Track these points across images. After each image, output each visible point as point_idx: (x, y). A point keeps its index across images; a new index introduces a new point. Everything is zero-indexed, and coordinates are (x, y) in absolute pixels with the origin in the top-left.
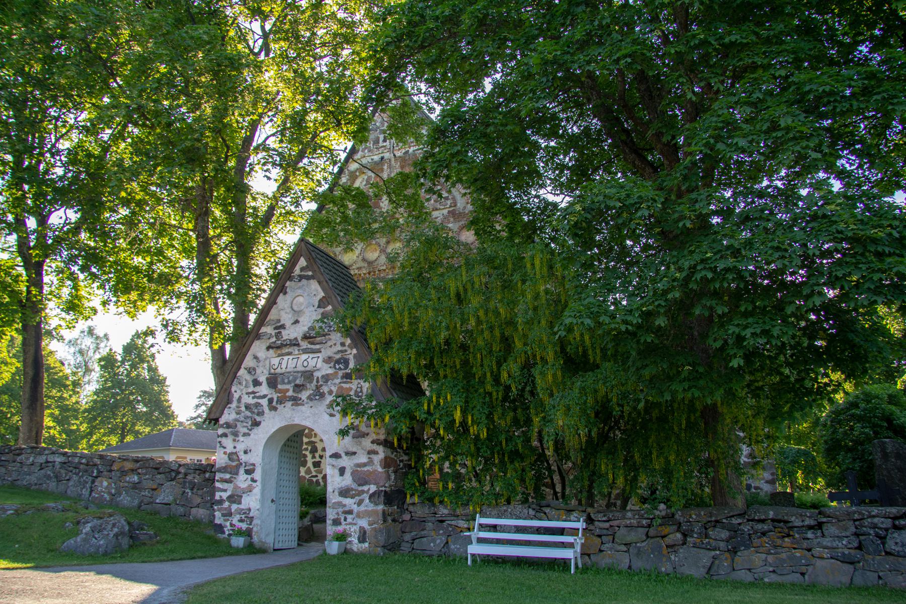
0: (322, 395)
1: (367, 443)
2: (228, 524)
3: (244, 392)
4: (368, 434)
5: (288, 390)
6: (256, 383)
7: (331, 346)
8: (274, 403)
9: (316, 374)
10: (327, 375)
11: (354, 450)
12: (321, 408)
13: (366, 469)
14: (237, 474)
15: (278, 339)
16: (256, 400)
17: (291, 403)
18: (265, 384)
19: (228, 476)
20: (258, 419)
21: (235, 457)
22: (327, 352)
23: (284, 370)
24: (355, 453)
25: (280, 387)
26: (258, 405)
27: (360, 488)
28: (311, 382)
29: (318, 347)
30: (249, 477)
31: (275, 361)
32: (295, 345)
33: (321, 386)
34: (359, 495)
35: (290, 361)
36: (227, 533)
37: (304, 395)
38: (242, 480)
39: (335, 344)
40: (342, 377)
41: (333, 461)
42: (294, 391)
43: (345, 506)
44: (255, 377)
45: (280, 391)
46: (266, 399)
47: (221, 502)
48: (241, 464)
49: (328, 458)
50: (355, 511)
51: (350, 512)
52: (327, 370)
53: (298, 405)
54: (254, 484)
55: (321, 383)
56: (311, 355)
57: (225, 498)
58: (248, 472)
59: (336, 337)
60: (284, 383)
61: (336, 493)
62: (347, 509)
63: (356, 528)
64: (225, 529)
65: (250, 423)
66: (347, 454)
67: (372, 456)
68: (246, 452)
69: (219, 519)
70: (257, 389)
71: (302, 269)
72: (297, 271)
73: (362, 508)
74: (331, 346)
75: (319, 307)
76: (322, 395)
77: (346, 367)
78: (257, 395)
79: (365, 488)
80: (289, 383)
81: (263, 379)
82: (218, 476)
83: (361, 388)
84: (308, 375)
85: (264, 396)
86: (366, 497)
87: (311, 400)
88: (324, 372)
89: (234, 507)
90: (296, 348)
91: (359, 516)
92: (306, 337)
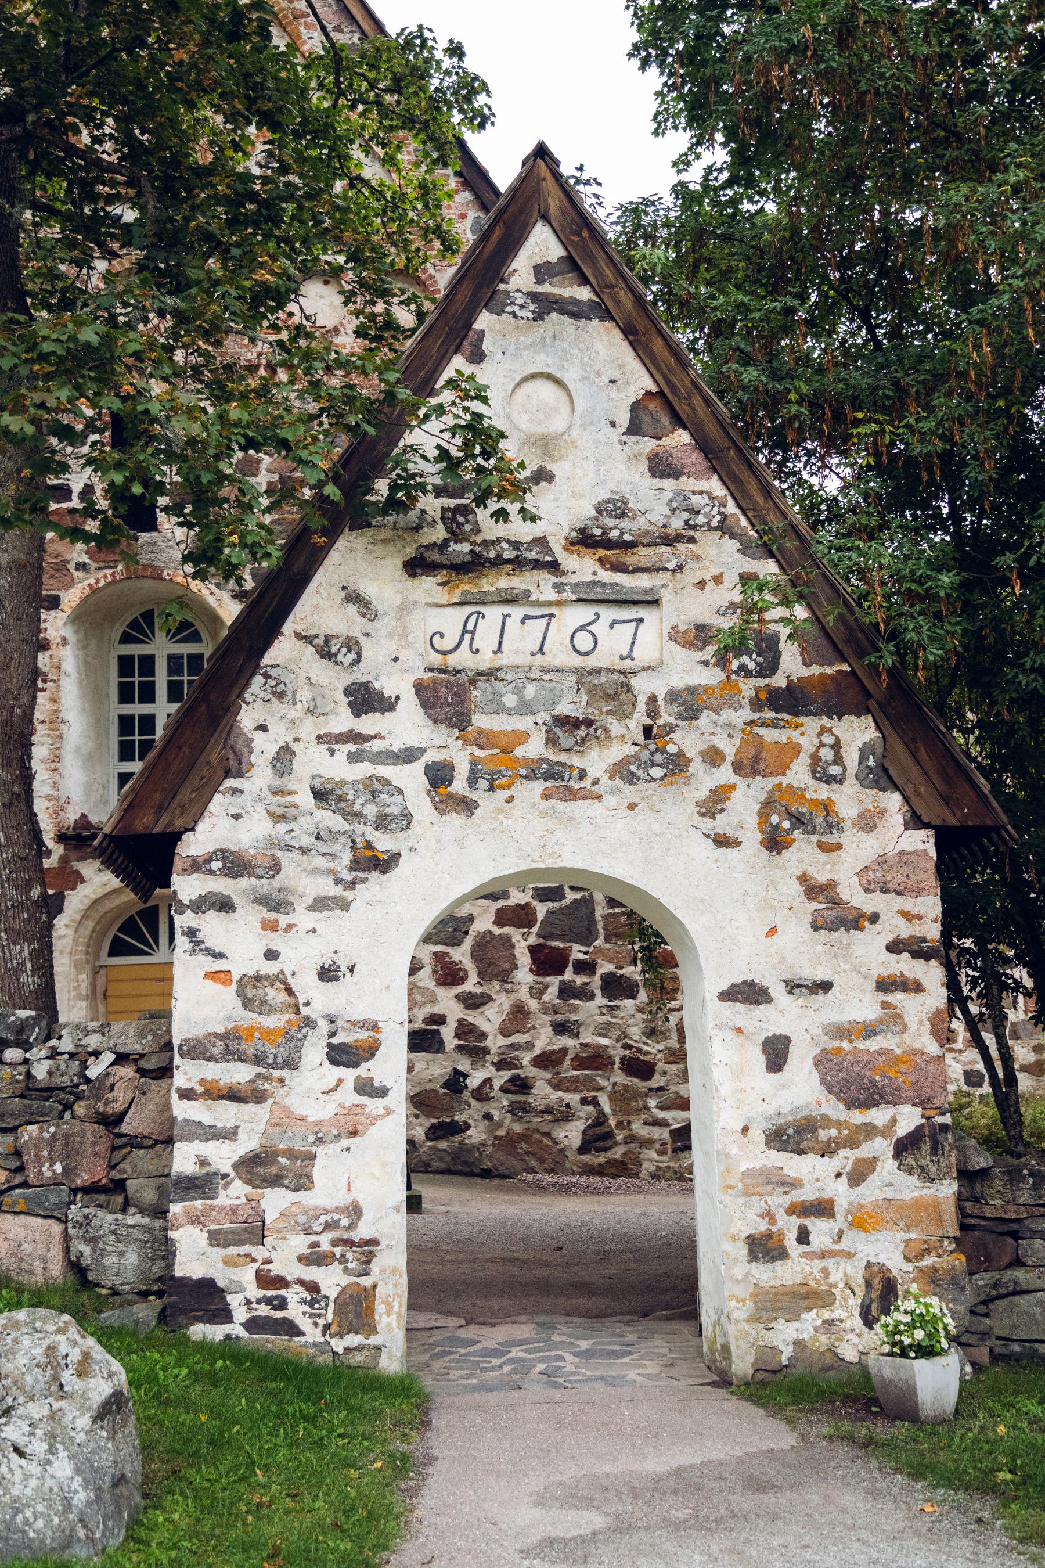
0: (677, 764)
1: (869, 951)
2: (247, 1275)
3: (309, 729)
4: (874, 918)
5: (522, 737)
6: (366, 699)
7: (701, 584)
8: (459, 786)
9: (643, 686)
10: (692, 691)
11: (821, 974)
12: (676, 809)
13: (873, 1044)
14: (291, 1064)
15: (455, 535)
16: (365, 769)
17: (538, 787)
18: (409, 705)
19: (240, 1074)
20: (384, 843)
21: (275, 995)
22: (691, 604)
23: (485, 660)
24: (825, 986)
25: (480, 721)
26: (375, 788)
27: (858, 1117)
28: (624, 716)
29: (643, 581)
30: (350, 1075)
31: (450, 622)
32: (537, 564)
33: (670, 729)
34: (852, 1143)
35: (513, 624)
36: (240, 1314)
37: (597, 762)
38: (314, 1089)
39: (718, 579)
40: (756, 704)
41: (739, 1013)
42: (551, 741)
43: (794, 1184)
44: (359, 676)
45: (484, 740)
46: (418, 768)
47: (202, 1185)
48: (309, 1023)
49: (714, 1005)
50: (841, 1206)
51: (823, 1209)
52: (690, 670)
53: (570, 795)
54: (374, 1105)
55: (666, 718)
56: (609, 614)
57: (225, 1167)
58: (341, 1055)
59: (724, 557)
60: (500, 709)
61: (757, 1135)
62: (807, 1194)
63: (856, 1272)
64: (234, 1301)
65: (347, 857)
66: (793, 987)
67: (897, 998)
68: (327, 974)
69: (194, 1256)
70: (368, 724)
71: (542, 272)
72: (520, 274)
73: (871, 1191)
74: (701, 584)
75: (634, 428)
76: (677, 764)
77: (770, 667)
78: (375, 746)
79: (879, 1116)
80: (525, 708)
81: (398, 683)
82: (187, 1073)
83: (836, 746)
84: (613, 689)
85: (408, 756)
86: (882, 1147)
87: (631, 779)
88: (678, 681)
89: (275, 1202)
90: (547, 580)
91: (860, 1221)
92: (584, 540)
